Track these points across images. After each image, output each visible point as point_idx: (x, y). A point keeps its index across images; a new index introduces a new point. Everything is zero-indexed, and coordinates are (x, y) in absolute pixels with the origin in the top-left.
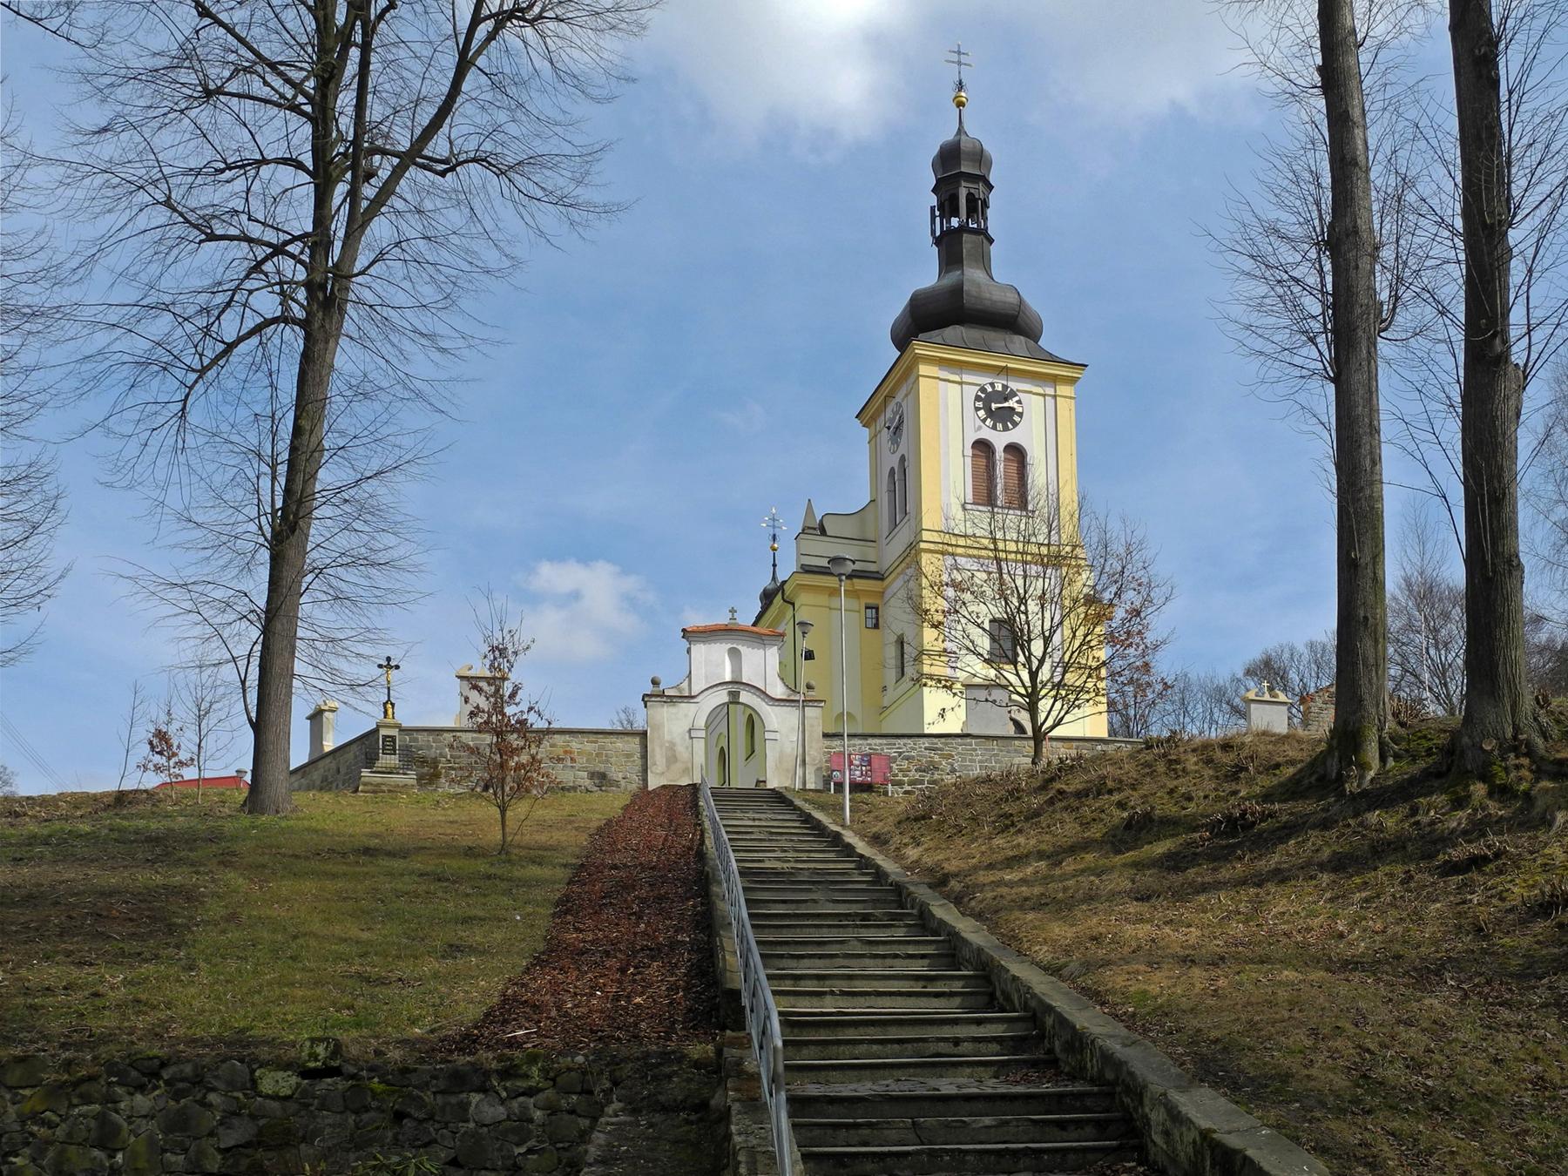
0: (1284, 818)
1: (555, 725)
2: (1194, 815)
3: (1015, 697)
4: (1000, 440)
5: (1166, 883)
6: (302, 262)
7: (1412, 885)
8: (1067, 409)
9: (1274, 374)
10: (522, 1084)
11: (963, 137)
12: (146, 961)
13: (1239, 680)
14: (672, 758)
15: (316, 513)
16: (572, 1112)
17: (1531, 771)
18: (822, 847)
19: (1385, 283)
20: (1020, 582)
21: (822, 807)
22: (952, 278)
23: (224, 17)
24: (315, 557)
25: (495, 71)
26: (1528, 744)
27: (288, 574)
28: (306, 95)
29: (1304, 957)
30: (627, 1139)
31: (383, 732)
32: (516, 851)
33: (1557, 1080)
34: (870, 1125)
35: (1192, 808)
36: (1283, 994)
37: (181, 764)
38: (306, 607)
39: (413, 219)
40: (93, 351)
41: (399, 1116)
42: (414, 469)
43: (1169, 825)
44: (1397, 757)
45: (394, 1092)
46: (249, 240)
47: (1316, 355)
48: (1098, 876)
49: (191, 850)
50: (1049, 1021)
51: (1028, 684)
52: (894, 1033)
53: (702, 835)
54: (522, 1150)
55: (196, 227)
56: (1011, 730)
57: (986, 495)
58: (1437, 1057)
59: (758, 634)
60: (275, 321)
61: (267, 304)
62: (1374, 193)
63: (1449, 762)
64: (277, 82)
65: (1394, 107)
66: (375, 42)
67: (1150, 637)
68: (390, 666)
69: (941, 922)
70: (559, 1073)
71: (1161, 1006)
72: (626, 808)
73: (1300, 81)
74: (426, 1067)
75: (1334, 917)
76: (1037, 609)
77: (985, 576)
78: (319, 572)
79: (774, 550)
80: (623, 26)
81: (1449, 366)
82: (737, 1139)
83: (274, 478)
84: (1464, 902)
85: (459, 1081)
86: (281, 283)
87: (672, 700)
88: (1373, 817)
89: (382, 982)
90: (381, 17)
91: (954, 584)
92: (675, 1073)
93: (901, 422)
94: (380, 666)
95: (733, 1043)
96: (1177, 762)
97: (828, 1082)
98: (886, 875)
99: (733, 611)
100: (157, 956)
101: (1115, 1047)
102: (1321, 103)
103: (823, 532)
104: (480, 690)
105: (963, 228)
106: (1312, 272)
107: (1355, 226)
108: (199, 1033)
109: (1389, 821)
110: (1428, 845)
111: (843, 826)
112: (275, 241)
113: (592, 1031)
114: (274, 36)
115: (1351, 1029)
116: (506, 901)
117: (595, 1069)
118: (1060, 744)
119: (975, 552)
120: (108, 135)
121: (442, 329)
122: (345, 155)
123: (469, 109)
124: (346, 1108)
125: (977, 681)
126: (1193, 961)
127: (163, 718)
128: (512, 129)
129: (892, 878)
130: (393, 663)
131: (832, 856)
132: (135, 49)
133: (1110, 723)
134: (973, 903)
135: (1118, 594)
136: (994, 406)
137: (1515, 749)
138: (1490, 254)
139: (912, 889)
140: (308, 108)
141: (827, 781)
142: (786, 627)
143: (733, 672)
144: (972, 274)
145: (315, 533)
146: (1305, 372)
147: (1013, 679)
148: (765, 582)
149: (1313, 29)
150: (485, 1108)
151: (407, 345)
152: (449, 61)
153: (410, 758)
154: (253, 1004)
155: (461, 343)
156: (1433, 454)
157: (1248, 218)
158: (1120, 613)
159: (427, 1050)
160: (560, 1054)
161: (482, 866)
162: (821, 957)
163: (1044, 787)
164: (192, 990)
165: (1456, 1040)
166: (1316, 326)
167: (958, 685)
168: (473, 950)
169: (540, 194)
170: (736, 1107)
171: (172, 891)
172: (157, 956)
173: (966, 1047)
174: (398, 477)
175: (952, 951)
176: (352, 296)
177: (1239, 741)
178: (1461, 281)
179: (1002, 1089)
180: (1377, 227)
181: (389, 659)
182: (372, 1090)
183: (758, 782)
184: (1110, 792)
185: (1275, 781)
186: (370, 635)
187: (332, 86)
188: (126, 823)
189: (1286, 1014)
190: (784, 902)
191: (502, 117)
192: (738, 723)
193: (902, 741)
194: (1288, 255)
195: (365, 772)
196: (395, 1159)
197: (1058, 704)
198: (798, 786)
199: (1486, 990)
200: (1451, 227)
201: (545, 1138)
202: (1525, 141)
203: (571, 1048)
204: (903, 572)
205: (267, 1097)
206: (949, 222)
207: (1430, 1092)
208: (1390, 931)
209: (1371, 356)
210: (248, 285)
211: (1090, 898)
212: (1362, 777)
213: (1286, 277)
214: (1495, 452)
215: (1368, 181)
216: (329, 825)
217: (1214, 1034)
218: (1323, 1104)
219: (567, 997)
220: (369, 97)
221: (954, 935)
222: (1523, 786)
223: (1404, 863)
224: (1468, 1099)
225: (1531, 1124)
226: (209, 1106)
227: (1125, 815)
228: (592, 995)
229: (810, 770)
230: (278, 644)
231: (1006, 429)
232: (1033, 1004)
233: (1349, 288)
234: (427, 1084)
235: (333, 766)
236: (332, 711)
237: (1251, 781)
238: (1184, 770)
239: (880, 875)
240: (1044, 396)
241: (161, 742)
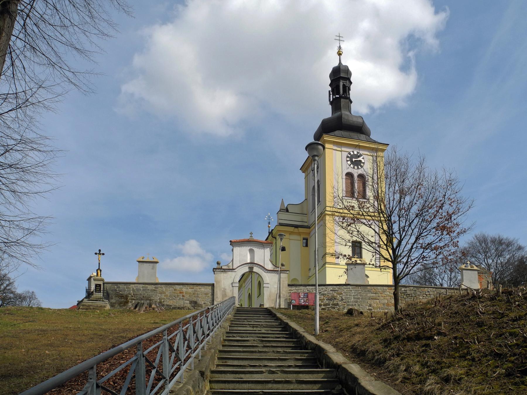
4: (356, 172)
22: (338, 114)
57: (351, 193)
87: (225, 271)
99: (251, 234)
103: (287, 210)
105: (341, 97)
130: (98, 252)
136: (354, 160)
141: (289, 304)
143: (251, 259)
181: (100, 251)
183: (261, 305)
192: (250, 278)
229: (282, 300)
231: (358, 168)
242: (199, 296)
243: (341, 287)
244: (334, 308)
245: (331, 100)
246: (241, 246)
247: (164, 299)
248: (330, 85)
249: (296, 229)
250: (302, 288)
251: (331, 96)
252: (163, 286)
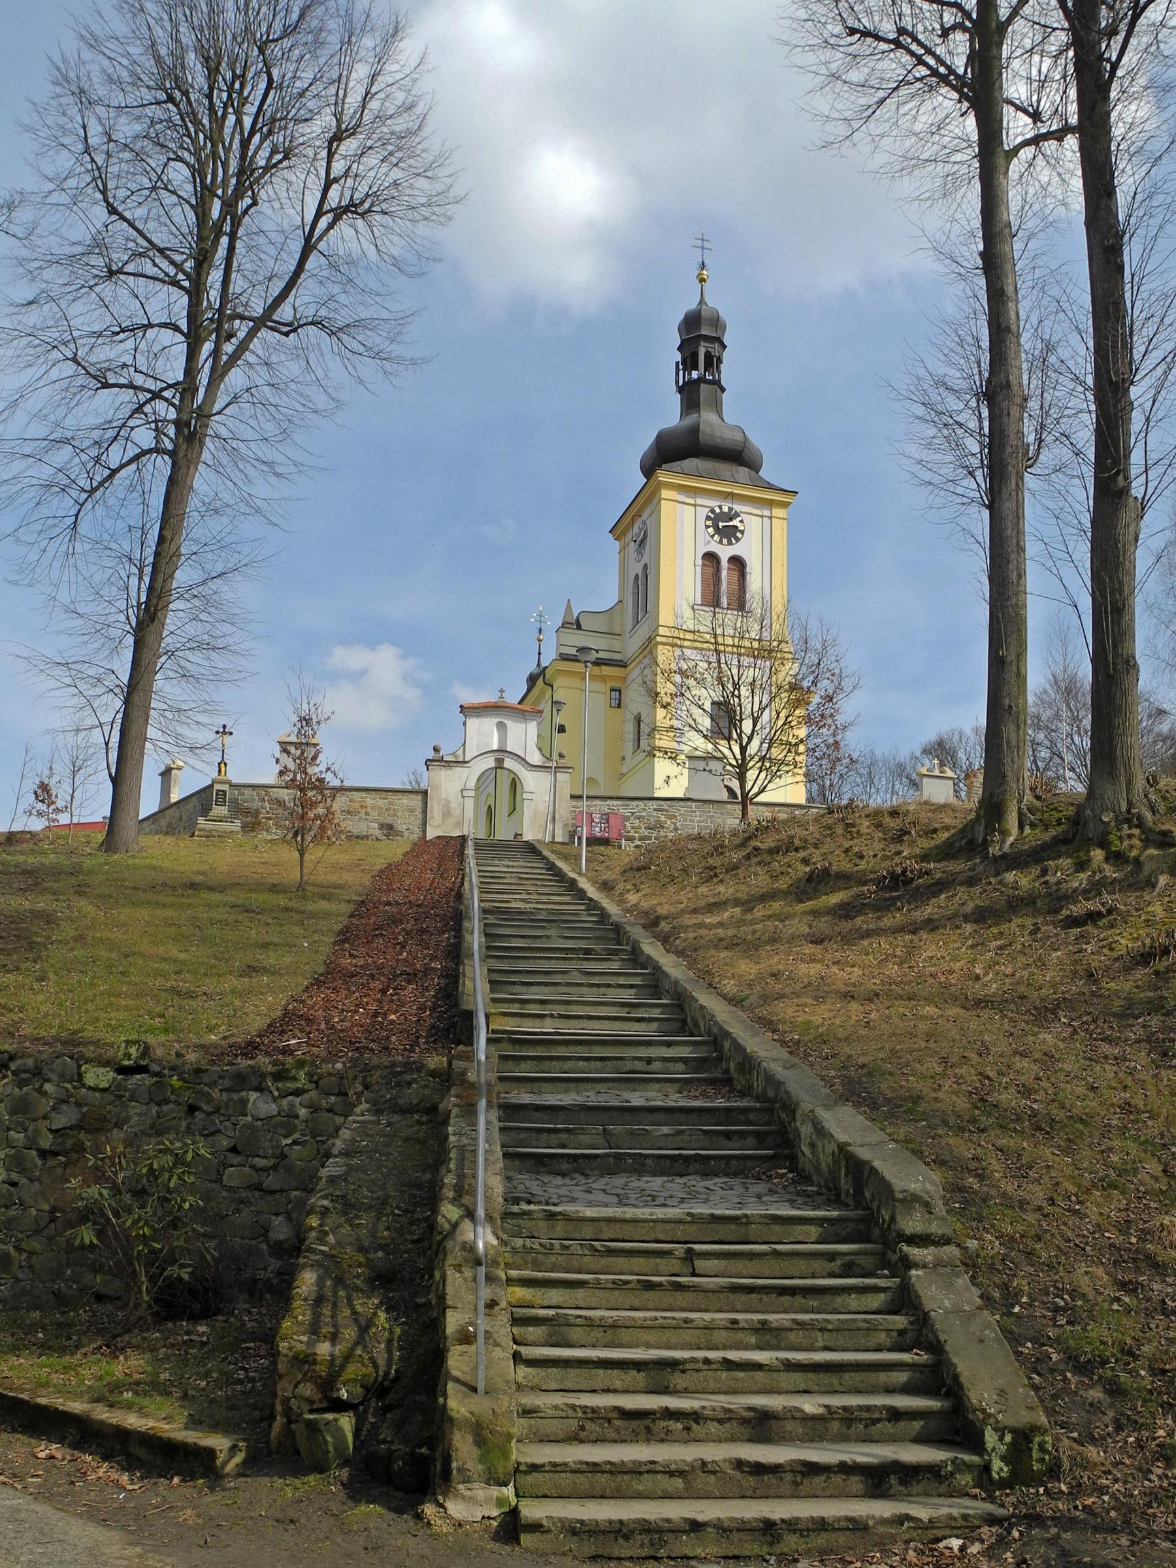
0: (938, 876)
1: (347, 784)
2: (864, 871)
3: (728, 767)
4: (725, 553)
5: (837, 929)
6: (173, 405)
7: (1039, 936)
8: (780, 528)
9: (940, 501)
10: (291, 1085)
11: (704, 307)
12: (9, 972)
13: (916, 758)
14: (447, 814)
15: (172, 607)
16: (330, 1110)
17: (1141, 840)
18: (560, 891)
19: (1032, 428)
20: (735, 671)
21: (565, 857)
22: (691, 419)
23: (127, 214)
24: (168, 642)
25: (331, 253)
26: (1139, 817)
27: (146, 655)
28: (184, 273)
29: (945, 996)
30: (368, 1135)
31: (217, 787)
32: (310, 888)
33: (1141, 1105)
34: (568, 1131)
35: (863, 865)
36: (923, 1026)
37: (57, 810)
38: (159, 683)
39: (262, 370)
40: (9, 476)
41: (192, 1109)
42: (250, 571)
43: (844, 879)
44: (1033, 825)
45: (189, 1088)
46: (135, 388)
47: (974, 486)
48: (782, 921)
49: (55, 881)
50: (727, 1045)
51: (739, 756)
52: (598, 1052)
53: (463, 878)
54: (289, 1141)
55: (94, 377)
56: (724, 795)
57: (712, 599)
58: (1044, 1084)
59: (522, 711)
60: (150, 451)
61: (144, 437)
62: (1023, 355)
63: (1076, 832)
64: (164, 264)
65: (1040, 286)
66: (240, 233)
67: (840, 719)
68: (224, 734)
69: (649, 958)
70: (321, 1077)
71: (822, 1034)
72: (406, 854)
73: (965, 264)
74: (215, 1068)
75: (974, 961)
76: (748, 693)
77: (705, 665)
78: (171, 654)
79: (540, 640)
80: (434, 217)
81: (1081, 496)
82: (452, 1138)
83: (141, 578)
84: (1080, 951)
85: (241, 1081)
86: (156, 421)
87: (449, 764)
88: (1010, 876)
89: (191, 995)
90: (246, 212)
91: (681, 672)
92: (415, 1080)
93: (645, 536)
94: (217, 732)
95: (460, 1057)
96: (853, 825)
97: (540, 1093)
98: (609, 916)
99: (502, 691)
100: (18, 969)
101: (777, 1070)
102: (982, 282)
103: (579, 627)
104: (288, 753)
105: (701, 380)
106: (973, 418)
107: (1008, 381)
108: (42, 1033)
109: (1022, 880)
110: (1057, 899)
111: (579, 874)
112: (153, 388)
113: (350, 1042)
114: (164, 228)
115: (975, 1058)
116: (298, 930)
117: (351, 1075)
118: (764, 808)
119: (699, 645)
120: (34, 306)
121: (278, 458)
122: (211, 320)
123: (310, 283)
124: (151, 1100)
125: (697, 753)
126: (852, 997)
127: (46, 772)
128: (343, 299)
129: (614, 918)
130: (221, 730)
131: (567, 899)
132: (58, 240)
133: (809, 792)
134: (678, 942)
135: (814, 683)
136: (721, 524)
137: (1128, 821)
138: (1115, 406)
139: (628, 928)
140: (186, 284)
141: (572, 835)
142: (546, 706)
143: (500, 741)
144: (707, 417)
145: (171, 622)
146: (965, 500)
147: (727, 752)
148: (532, 668)
149: (977, 223)
150: (261, 1104)
151: (250, 471)
152: (297, 246)
153: (237, 810)
154: (87, 1011)
155: (293, 469)
156: (1067, 572)
157: (922, 372)
158: (815, 699)
159: (216, 1054)
160: (323, 1061)
161: (282, 901)
162: (547, 984)
163: (743, 844)
164: (41, 997)
165: (1061, 1069)
166: (976, 462)
167: (682, 757)
168: (266, 970)
169: (362, 349)
170: (455, 1111)
171: (36, 915)
172: (18, 969)
173: (656, 1065)
174: (237, 576)
175: (656, 983)
176: (210, 431)
177: (904, 808)
178: (1091, 427)
179: (683, 1103)
180: (1025, 382)
181: (224, 727)
182: (171, 1086)
183: (516, 835)
184: (797, 850)
185: (932, 843)
186: (207, 707)
187: (205, 265)
188: (9, 858)
189: (923, 1045)
190: (523, 937)
191: (336, 289)
192: (502, 784)
193: (634, 803)
194: (953, 404)
195: (201, 820)
196: (178, 1144)
197: (763, 774)
198: (548, 839)
199: (1092, 1027)
200: (1082, 383)
201: (308, 1132)
202: (1143, 315)
203: (332, 1056)
204: (641, 662)
205: (90, 1088)
206: (690, 374)
207: (1035, 1114)
208: (1018, 975)
209: (1019, 487)
210: (131, 423)
211: (773, 940)
212: (1003, 842)
213: (951, 422)
214: (1117, 569)
215: (1019, 344)
216: (166, 864)
217: (861, 1060)
218: (945, 1123)
219: (335, 1013)
220: (233, 275)
221: (657, 969)
222: (1134, 853)
223: (1034, 916)
224: (1066, 1121)
225: (1115, 1143)
226: (44, 1094)
227: (808, 869)
228: (356, 1011)
230: (135, 714)
231: (730, 543)
232: (715, 1030)
233: (1002, 432)
234: (215, 1083)
235: (177, 815)
236: (179, 768)
237: (912, 843)
238: (858, 833)
239: (604, 916)
240: (762, 516)
241: (44, 792)
243: (674, 803)
249: (596, 668)
250: (598, 802)
251: (681, 373)
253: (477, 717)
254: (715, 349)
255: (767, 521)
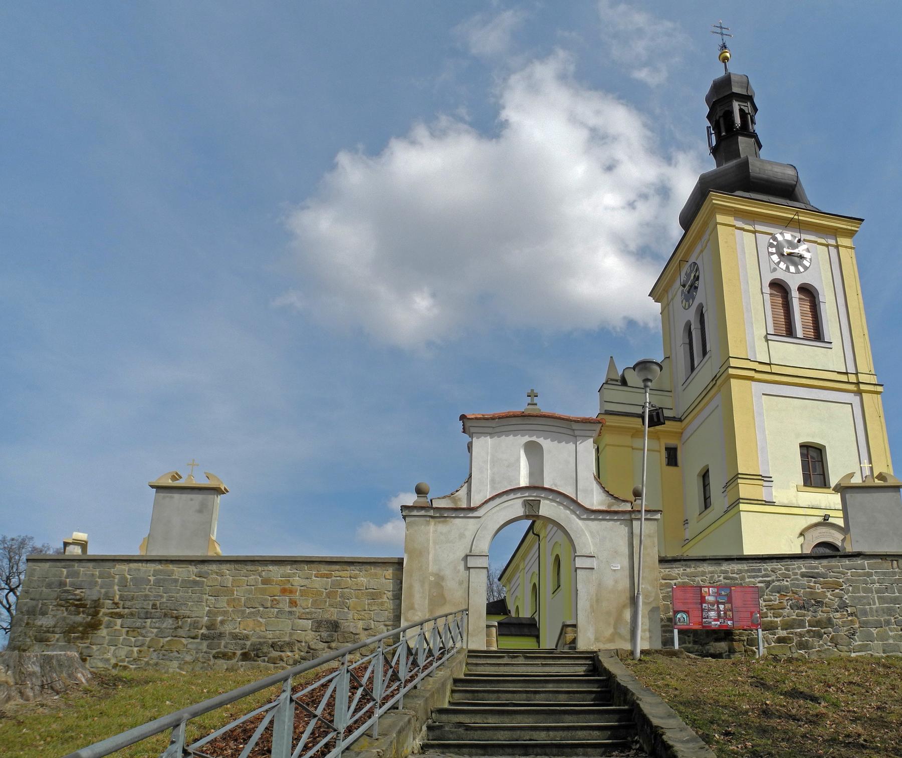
14: (438, 596)
87: (442, 515)
103: (624, 382)
141: (668, 625)
143: (531, 475)
193: (769, 566)
242: (350, 602)
244: (820, 636)
245: (714, 143)
246: (499, 434)
247: (225, 613)
248: (709, 117)
250: (707, 568)
252: (225, 568)
253: (491, 435)
254: (748, 108)
255: (833, 251)
